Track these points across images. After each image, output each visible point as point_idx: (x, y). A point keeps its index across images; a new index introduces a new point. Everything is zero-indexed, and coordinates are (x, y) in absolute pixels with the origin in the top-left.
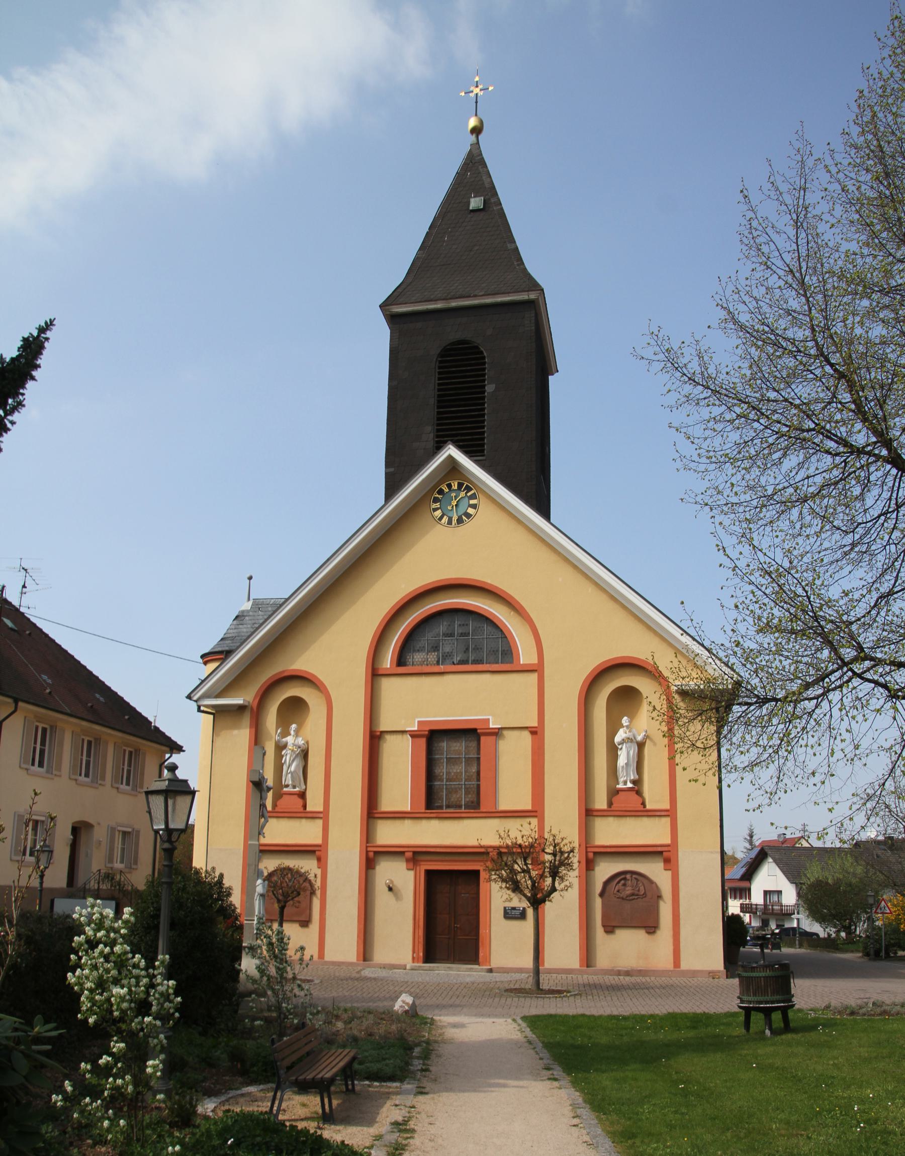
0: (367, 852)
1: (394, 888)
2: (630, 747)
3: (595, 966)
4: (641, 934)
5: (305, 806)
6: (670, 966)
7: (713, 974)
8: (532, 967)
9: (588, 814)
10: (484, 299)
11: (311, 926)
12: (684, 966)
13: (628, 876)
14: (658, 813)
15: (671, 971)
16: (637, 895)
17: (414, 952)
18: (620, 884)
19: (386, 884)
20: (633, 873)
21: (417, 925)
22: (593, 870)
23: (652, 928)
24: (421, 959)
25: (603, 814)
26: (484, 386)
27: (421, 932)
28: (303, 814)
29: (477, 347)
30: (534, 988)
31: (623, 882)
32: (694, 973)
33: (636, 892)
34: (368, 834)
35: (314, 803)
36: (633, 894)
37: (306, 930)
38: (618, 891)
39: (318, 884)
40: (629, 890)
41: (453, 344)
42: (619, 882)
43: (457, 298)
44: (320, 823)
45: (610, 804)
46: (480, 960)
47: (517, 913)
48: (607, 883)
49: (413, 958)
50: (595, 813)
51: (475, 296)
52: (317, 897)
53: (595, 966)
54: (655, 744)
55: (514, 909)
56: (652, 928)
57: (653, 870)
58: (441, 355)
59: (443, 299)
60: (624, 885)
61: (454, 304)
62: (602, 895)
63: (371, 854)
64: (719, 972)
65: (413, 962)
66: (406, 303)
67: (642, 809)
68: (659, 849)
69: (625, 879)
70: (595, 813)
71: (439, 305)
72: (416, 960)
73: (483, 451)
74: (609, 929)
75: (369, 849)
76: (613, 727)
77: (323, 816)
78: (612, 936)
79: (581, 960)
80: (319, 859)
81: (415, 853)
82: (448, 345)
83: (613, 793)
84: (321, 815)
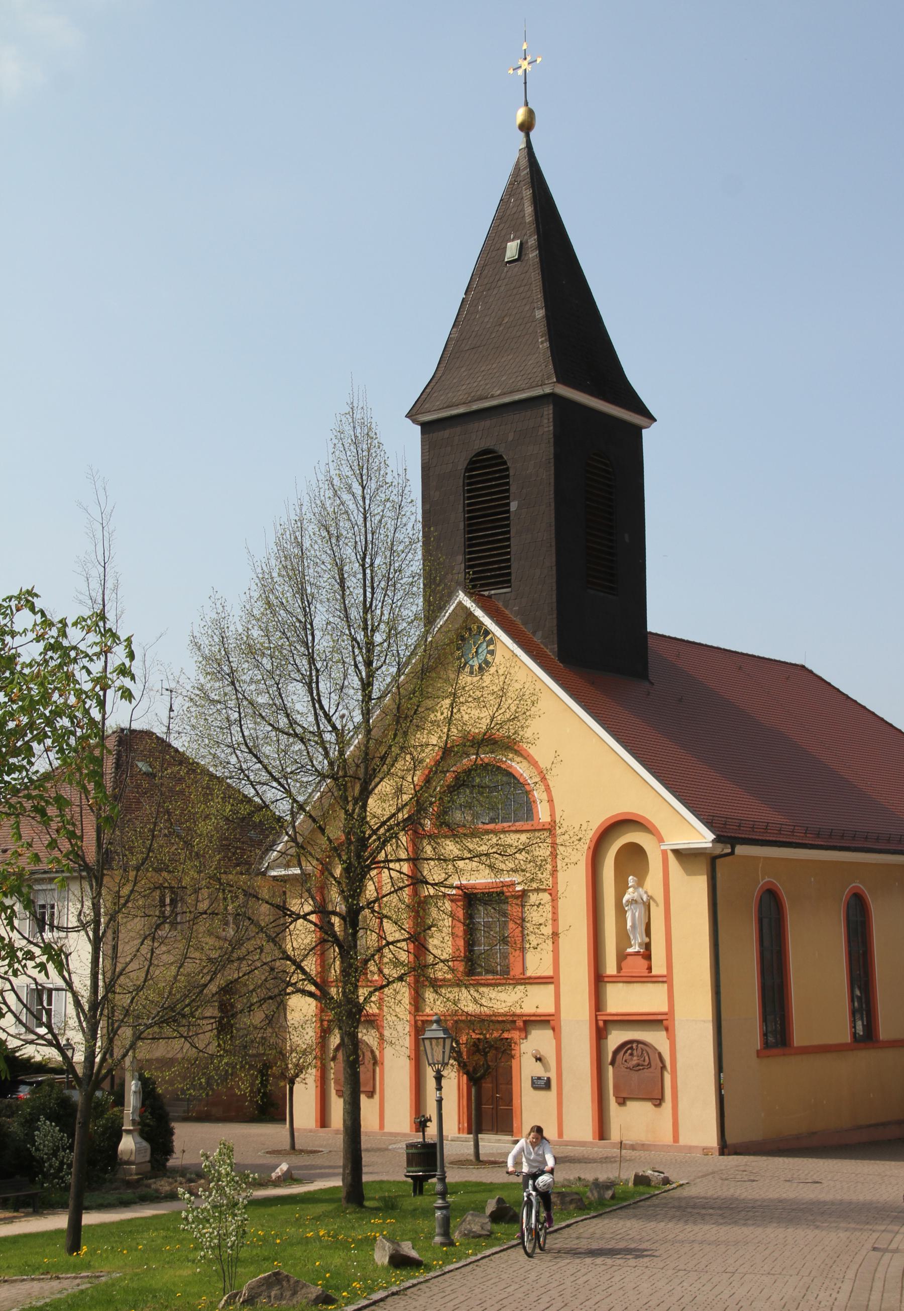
0: (597, 1021)
1: (543, 1059)
2: (636, 909)
3: (610, 1139)
4: (648, 1106)
5: (650, 969)
6: (668, 1139)
7: (706, 1151)
8: (436, 1133)
9: (599, 980)
10: (502, 398)
11: (664, 1105)
12: (683, 1141)
13: (634, 1045)
14: (661, 979)
15: (670, 1146)
16: (642, 1065)
17: (459, 1123)
18: (627, 1054)
19: (533, 1055)
20: (638, 1042)
21: (461, 1095)
22: (606, 1038)
23: (658, 1101)
24: (466, 1130)
25: (615, 980)
26: (508, 504)
27: (719, 1112)
28: (648, 978)
29: (501, 457)
30: (472, 1158)
31: (629, 1051)
32: (690, 1149)
33: (641, 1063)
34: (598, 1001)
35: (658, 968)
36: (638, 1065)
37: (372, 1100)
38: (626, 1061)
39: (437, 1052)
40: (635, 1060)
41: (479, 454)
42: (626, 1052)
43: (475, 401)
44: (552, 987)
45: (619, 968)
46: (515, 1130)
47: (542, 1082)
48: (616, 1052)
49: (459, 1129)
50: (606, 979)
51: (492, 396)
52: (667, 1071)
53: (610, 1139)
54: (657, 905)
55: (539, 1078)
56: (658, 1101)
57: (656, 1039)
58: (467, 470)
59: (464, 404)
60: (631, 1054)
61: (475, 407)
62: (613, 1063)
63: (601, 1024)
64: (712, 1148)
65: (459, 1133)
66: (429, 412)
67: (646, 974)
68: (659, 1017)
69: (631, 1048)
70: (606, 979)
71: (461, 410)
72: (461, 1131)
73: (509, 581)
74: (622, 1102)
75: (418, 1018)
76: (621, 888)
77: (666, 980)
78: (623, 1108)
79: (594, 1133)
80: (553, 1029)
81: (525, 1022)
82: (474, 457)
83: (622, 957)
84: (665, 979)
